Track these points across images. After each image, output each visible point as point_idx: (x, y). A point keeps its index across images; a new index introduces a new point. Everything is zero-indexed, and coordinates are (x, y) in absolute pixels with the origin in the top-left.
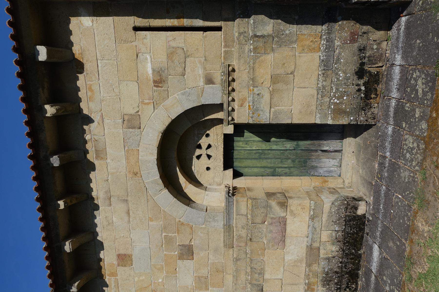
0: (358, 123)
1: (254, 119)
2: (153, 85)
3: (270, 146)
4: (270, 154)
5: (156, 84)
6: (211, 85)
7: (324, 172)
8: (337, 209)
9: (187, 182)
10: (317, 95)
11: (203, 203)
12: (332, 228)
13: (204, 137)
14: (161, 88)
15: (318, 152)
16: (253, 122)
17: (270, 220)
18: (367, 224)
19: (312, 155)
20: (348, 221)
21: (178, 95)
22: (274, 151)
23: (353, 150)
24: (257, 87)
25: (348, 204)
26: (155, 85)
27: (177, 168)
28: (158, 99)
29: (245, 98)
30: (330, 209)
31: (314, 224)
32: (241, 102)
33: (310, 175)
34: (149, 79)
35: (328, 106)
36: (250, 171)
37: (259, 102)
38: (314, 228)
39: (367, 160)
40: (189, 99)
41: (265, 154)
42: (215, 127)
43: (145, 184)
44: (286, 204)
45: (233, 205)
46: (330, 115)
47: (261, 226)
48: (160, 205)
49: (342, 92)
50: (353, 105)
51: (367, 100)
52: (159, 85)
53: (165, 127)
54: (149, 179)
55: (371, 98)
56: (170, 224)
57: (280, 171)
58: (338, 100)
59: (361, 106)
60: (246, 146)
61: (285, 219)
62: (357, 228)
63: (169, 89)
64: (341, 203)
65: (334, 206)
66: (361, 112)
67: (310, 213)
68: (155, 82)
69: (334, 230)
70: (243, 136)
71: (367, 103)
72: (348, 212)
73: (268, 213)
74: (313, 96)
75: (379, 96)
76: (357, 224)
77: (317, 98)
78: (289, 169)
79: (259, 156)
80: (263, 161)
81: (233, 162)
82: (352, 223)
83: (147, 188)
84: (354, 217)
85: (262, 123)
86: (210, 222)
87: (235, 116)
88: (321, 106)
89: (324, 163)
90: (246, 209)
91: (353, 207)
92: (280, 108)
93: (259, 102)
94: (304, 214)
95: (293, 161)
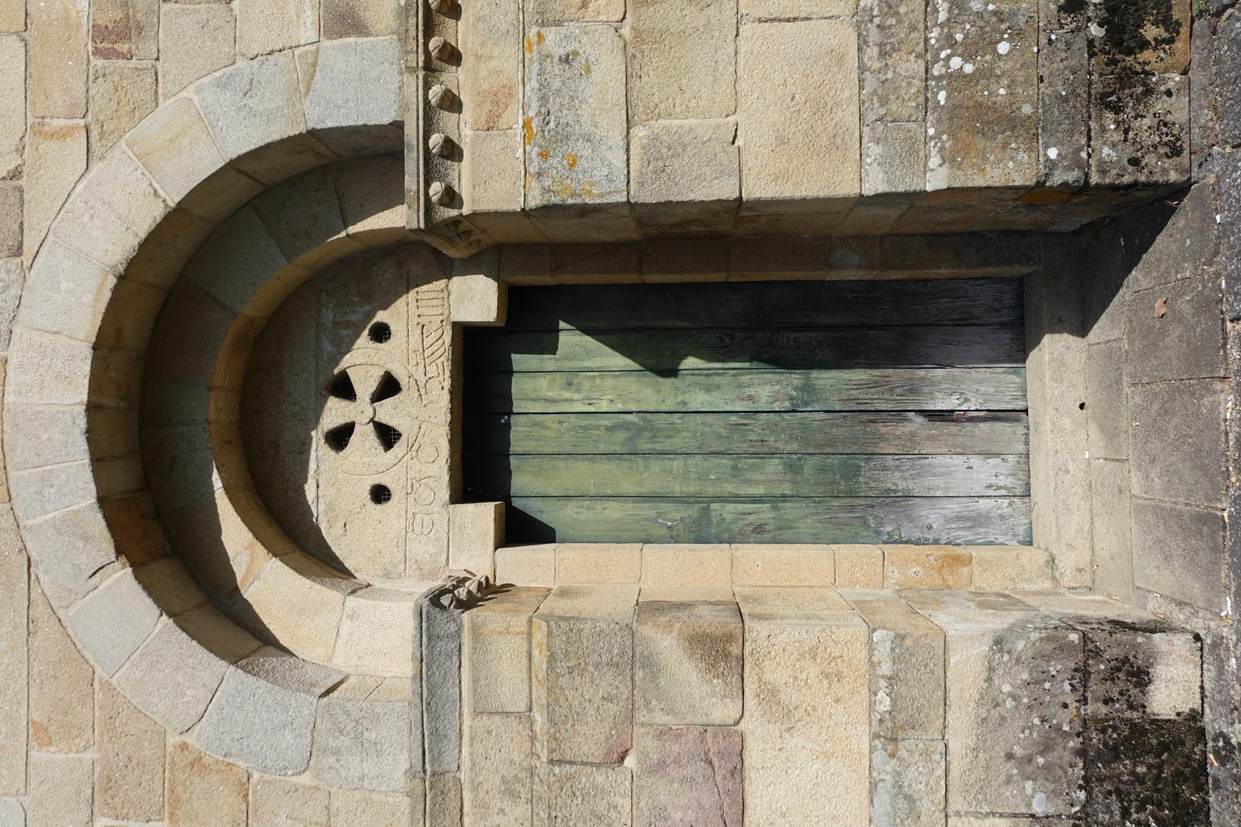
0: (1087, 175)
1: (547, 182)
2: (90, 49)
3: (676, 395)
4: (678, 431)
5: (106, 45)
6: (351, 40)
7: (949, 520)
8: (1025, 676)
9: (260, 549)
10: (860, 49)
11: (330, 660)
12: (1011, 799)
13: (364, 339)
14: (125, 61)
15: (910, 420)
16: (546, 197)
17: (650, 743)
18: (1222, 774)
19: (883, 438)
20: (1099, 756)
21: (198, 91)
22: (698, 416)
23: (1081, 395)
24: (559, 23)
25: (1090, 650)
26: (100, 46)
27: (215, 477)
28: (109, 113)
29: (504, 86)
30: (989, 680)
31: (899, 774)
32: (488, 106)
33: (877, 537)
34: (73, 21)
35: (921, 99)
36: (586, 515)
37: (572, 98)
38: (906, 797)
39: (1163, 405)
40: (251, 108)
41: (655, 433)
42: (412, 293)
43: (26, 537)
44: (735, 650)
45: (455, 659)
46: (932, 144)
47: (600, 779)
48: (87, 655)
49: (986, 16)
50: (1050, 84)
51: (1120, 53)
52: (115, 46)
53: (135, 242)
54: (46, 512)
55: (1144, 45)
56: (134, 761)
57: (729, 517)
58: (966, 61)
59: (1097, 88)
60: (567, 395)
61: (738, 739)
62: (1160, 806)
63: (159, 65)
64: (1048, 639)
65: (1006, 657)
66: (1100, 117)
67: (872, 705)
68: (99, 32)
69: (1023, 815)
70: (552, 349)
71: (1124, 68)
72: (1096, 700)
73: (640, 702)
74: (840, 60)
75: (1184, 30)
76: (1158, 778)
77: (862, 69)
78: (775, 509)
79: (627, 440)
80: (647, 468)
81: (508, 474)
82: (1124, 767)
83: (34, 556)
84: (1137, 730)
85: (588, 201)
86: (336, 752)
87: (463, 181)
88: (884, 101)
89: (942, 474)
90: (525, 676)
91: (1119, 670)
92: (676, 122)
93: (572, 98)
94: (840, 707)
95: (792, 468)
